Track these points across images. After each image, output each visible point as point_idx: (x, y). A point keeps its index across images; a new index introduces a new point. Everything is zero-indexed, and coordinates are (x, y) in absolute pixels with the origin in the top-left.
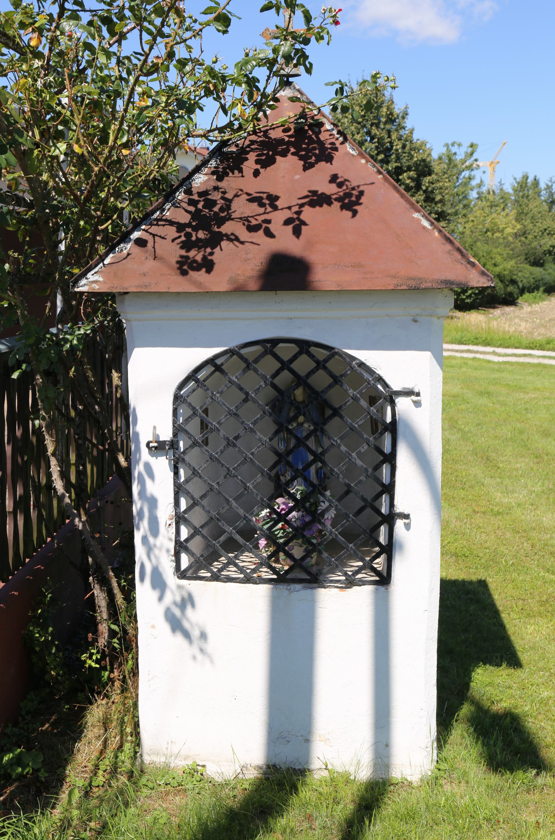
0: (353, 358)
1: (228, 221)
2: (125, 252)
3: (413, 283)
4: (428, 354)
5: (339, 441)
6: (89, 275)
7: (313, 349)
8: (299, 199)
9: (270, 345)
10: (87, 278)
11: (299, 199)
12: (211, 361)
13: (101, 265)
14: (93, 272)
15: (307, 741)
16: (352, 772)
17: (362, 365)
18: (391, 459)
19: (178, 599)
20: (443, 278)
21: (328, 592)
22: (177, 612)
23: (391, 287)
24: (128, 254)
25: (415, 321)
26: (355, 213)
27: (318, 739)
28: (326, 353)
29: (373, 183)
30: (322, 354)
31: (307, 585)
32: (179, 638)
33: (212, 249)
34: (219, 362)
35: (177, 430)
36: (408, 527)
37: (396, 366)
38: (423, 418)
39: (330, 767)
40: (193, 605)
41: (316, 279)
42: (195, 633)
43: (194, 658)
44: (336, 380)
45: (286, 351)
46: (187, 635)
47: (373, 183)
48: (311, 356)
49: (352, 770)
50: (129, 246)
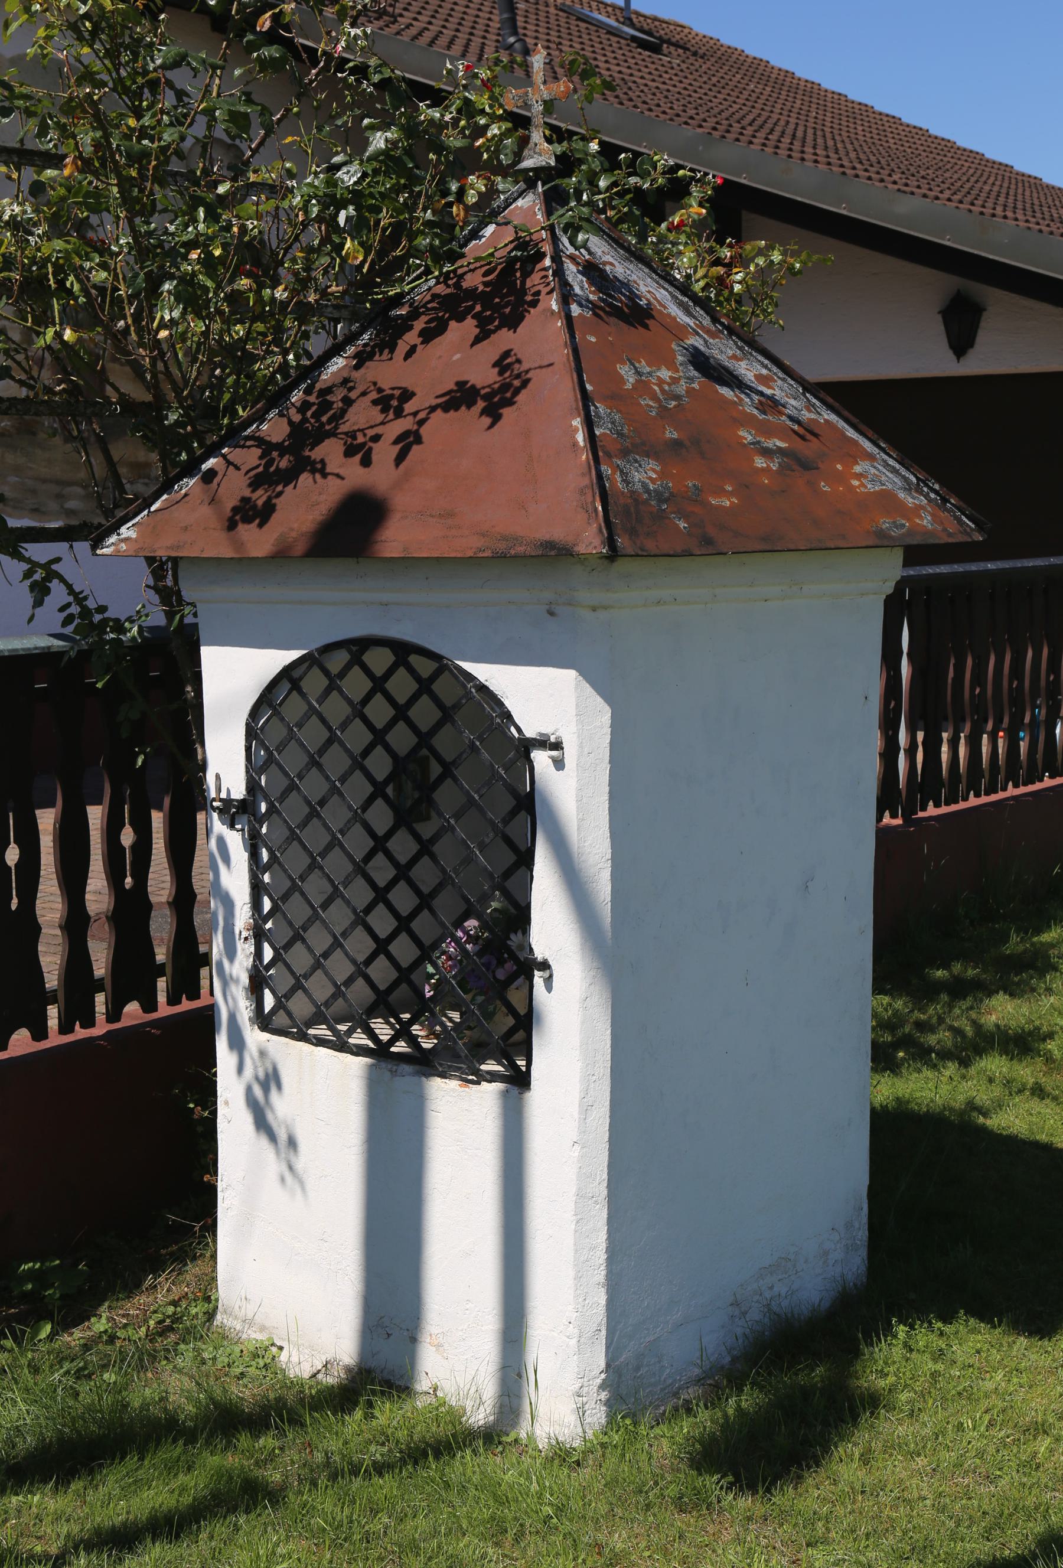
0: (470, 677)
1: (329, 437)
2: (183, 491)
3: (502, 546)
4: (572, 674)
5: (452, 821)
6: (123, 530)
7: (414, 659)
8: (437, 397)
9: (358, 647)
10: (119, 534)
11: (437, 397)
12: (287, 673)
13: (146, 512)
14: (130, 524)
15: (413, 1340)
16: (469, 1409)
17: (483, 689)
18: (526, 860)
19: (261, 1074)
20: (547, 537)
21: (443, 1085)
22: (258, 1091)
23: (470, 554)
24: (186, 495)
25: (551, 613)
26: (496, 418)
27: (428, 1340)
28: (435, 665)
29: (551, 365)
30: (425, 667)
31: (417, 1067)
32: (264, 1141)
33: (284, 487)
34: (296, 674)
35: (252, 786)
36: (549, 982)
37: (542, 697)
38: (575, 790)
39: (440, 1394)
40: (279, 1087)
41: (383, 538)
42: (282, 1136)
43: (283, 1180)
44: (447, 714)
45: (379, 660)
46: (272, 1137)
47: (551, 365)
48: (411, 670)
49: (469, 1405)
50: (192, 482)
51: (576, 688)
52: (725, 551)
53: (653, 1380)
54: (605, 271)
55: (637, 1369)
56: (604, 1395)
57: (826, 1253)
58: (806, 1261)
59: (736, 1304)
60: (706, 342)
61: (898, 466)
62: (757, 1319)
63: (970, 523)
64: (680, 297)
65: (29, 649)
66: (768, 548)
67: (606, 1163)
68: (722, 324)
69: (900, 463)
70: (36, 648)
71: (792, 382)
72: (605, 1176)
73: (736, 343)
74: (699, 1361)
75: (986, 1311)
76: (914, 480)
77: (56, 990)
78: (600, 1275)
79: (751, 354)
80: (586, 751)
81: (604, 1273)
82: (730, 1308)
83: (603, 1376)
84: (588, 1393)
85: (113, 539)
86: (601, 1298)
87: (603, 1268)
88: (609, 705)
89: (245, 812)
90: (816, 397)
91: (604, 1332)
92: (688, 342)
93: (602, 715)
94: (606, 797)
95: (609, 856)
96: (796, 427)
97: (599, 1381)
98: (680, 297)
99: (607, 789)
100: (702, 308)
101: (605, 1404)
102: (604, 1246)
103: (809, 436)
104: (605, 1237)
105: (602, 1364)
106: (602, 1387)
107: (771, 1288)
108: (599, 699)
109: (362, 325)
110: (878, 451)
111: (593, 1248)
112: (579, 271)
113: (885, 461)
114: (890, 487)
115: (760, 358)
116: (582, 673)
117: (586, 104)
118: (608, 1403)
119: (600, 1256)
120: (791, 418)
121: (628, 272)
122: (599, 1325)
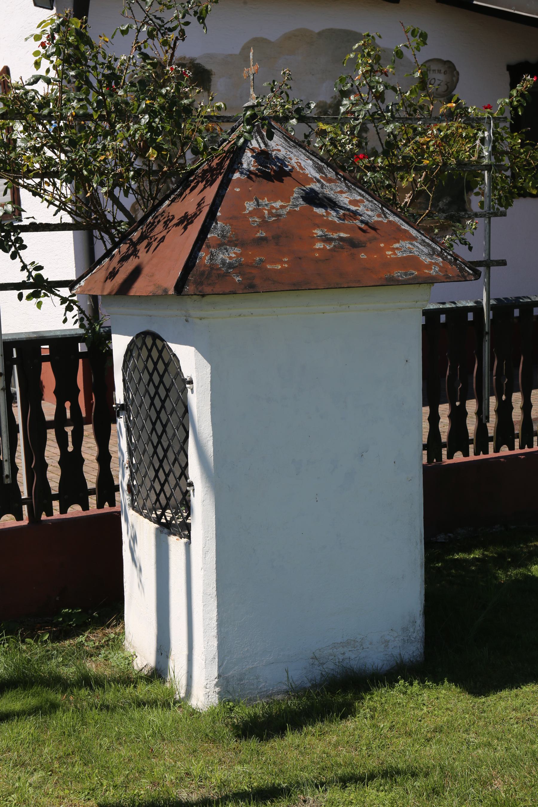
4: (193, 349)
25: (187, 321)
51: (195, 356)
52: (259, 291)
53: (252, 687)
54: (271, 154)
55: (241, 680)
56: (217, 689)
57: (387, 642)
58: (371, 644)
59: (315, 658)
60: (322, 185)
61: (431, 243)
62: (332, 668)
63: (470, 271)
64: (320, 163)
65: (73, 335)
66: (296, 289)
67: (215, 579)
68: (340, 175)
69: (432, 241)
70: (76, 334)
71: (376, 202)
72: (215, 585)
73: (346, 184)
74: (287, 683)
75: (457, 680)
76: (439, 249)
77: (95, 489)
78: (214, 632)
79: (355, 189)
80: (200, 385)
81: (216, 631)
82: (311, 660)
83: (217, 680)
84: (210, 687)
85: (77, 286)
86: (215, 643)
87: (215, 629)
88: (210, 364)
89: (123, 409)
90: (388, 209)
91: (217, 660)
92: (308, 186)
93: (207, 368)
94: (209, 407)
95: (211, 434)
96: (363, 226)
97: (214, 682)
98: (320, 163)
99: (210, 403)
100: (331, 168)
101: (218, 694)
102: (215, 618)
103: (370, 230)
104: (216, 614)
105: (216, 675)
106: (217, 685)
107: (344, 654)
108: (205, 361)
109: (177, 185)
110: (420, 235)
111: (211, 619)
112: (252, 156)
113: (424, 241)
114: (416, 253)
115: (360, 191)
116: (197, 348)
117: (416, 52)
118: (219, 693)
119: (214, 623)
120: (362, 222)
121: (288, 153)
122: (214, 656)
